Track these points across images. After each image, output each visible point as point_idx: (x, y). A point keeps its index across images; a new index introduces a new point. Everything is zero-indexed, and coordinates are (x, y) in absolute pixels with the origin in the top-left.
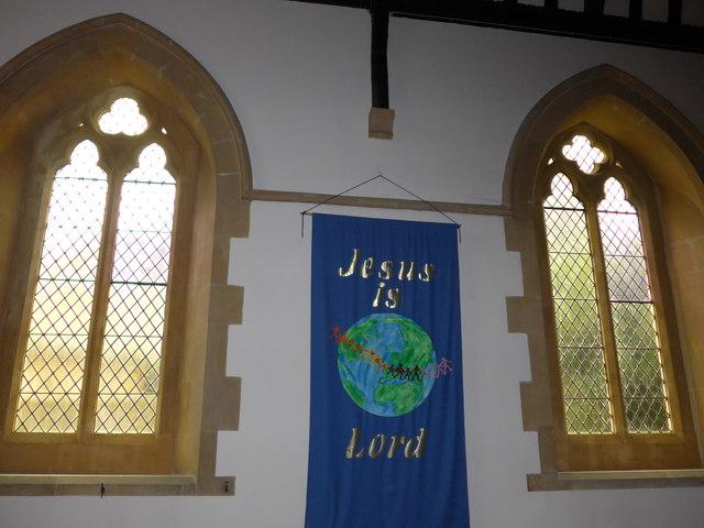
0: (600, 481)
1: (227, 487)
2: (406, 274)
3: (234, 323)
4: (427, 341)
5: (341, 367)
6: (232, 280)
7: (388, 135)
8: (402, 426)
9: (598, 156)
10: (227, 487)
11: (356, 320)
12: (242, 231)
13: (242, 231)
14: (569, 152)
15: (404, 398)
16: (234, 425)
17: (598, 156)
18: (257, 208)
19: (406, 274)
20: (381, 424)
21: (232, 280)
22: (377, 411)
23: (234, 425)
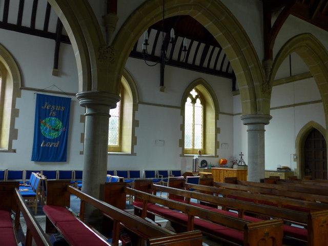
0: (20, 73)
1: (14, 151)
2: (58, 108)
3: (18, 97)
4: (61, 123)
5: (41, 128)
6: (16, 128)
7: (163, 91)
8: (55, 140)
9: (196, 94)
10: (14, 151)
11: (45, 118)
12: (20, 96)
13: (20, 96)
14: (191, 93)
15: (54, 135)
16: (16, 139)
17: (196, 94)
18: (23, 92)
19: (58, 108)
20: (49, 140)
21: (16, 128)
22: (48, 137)
23: (16, 139)
